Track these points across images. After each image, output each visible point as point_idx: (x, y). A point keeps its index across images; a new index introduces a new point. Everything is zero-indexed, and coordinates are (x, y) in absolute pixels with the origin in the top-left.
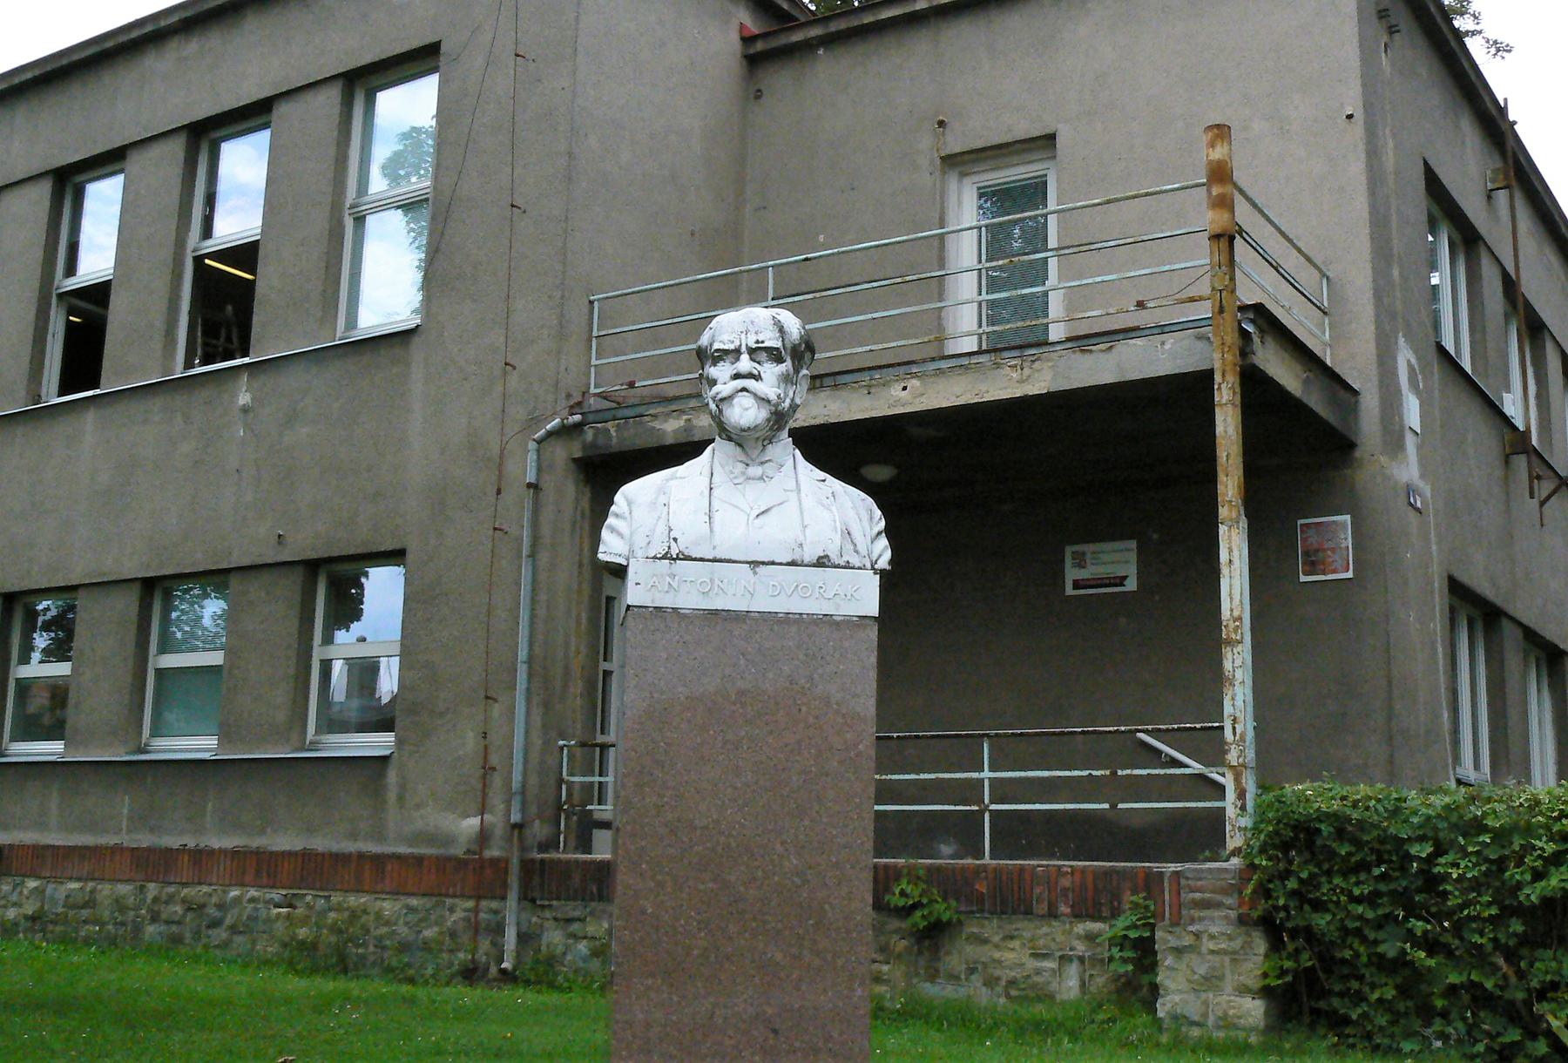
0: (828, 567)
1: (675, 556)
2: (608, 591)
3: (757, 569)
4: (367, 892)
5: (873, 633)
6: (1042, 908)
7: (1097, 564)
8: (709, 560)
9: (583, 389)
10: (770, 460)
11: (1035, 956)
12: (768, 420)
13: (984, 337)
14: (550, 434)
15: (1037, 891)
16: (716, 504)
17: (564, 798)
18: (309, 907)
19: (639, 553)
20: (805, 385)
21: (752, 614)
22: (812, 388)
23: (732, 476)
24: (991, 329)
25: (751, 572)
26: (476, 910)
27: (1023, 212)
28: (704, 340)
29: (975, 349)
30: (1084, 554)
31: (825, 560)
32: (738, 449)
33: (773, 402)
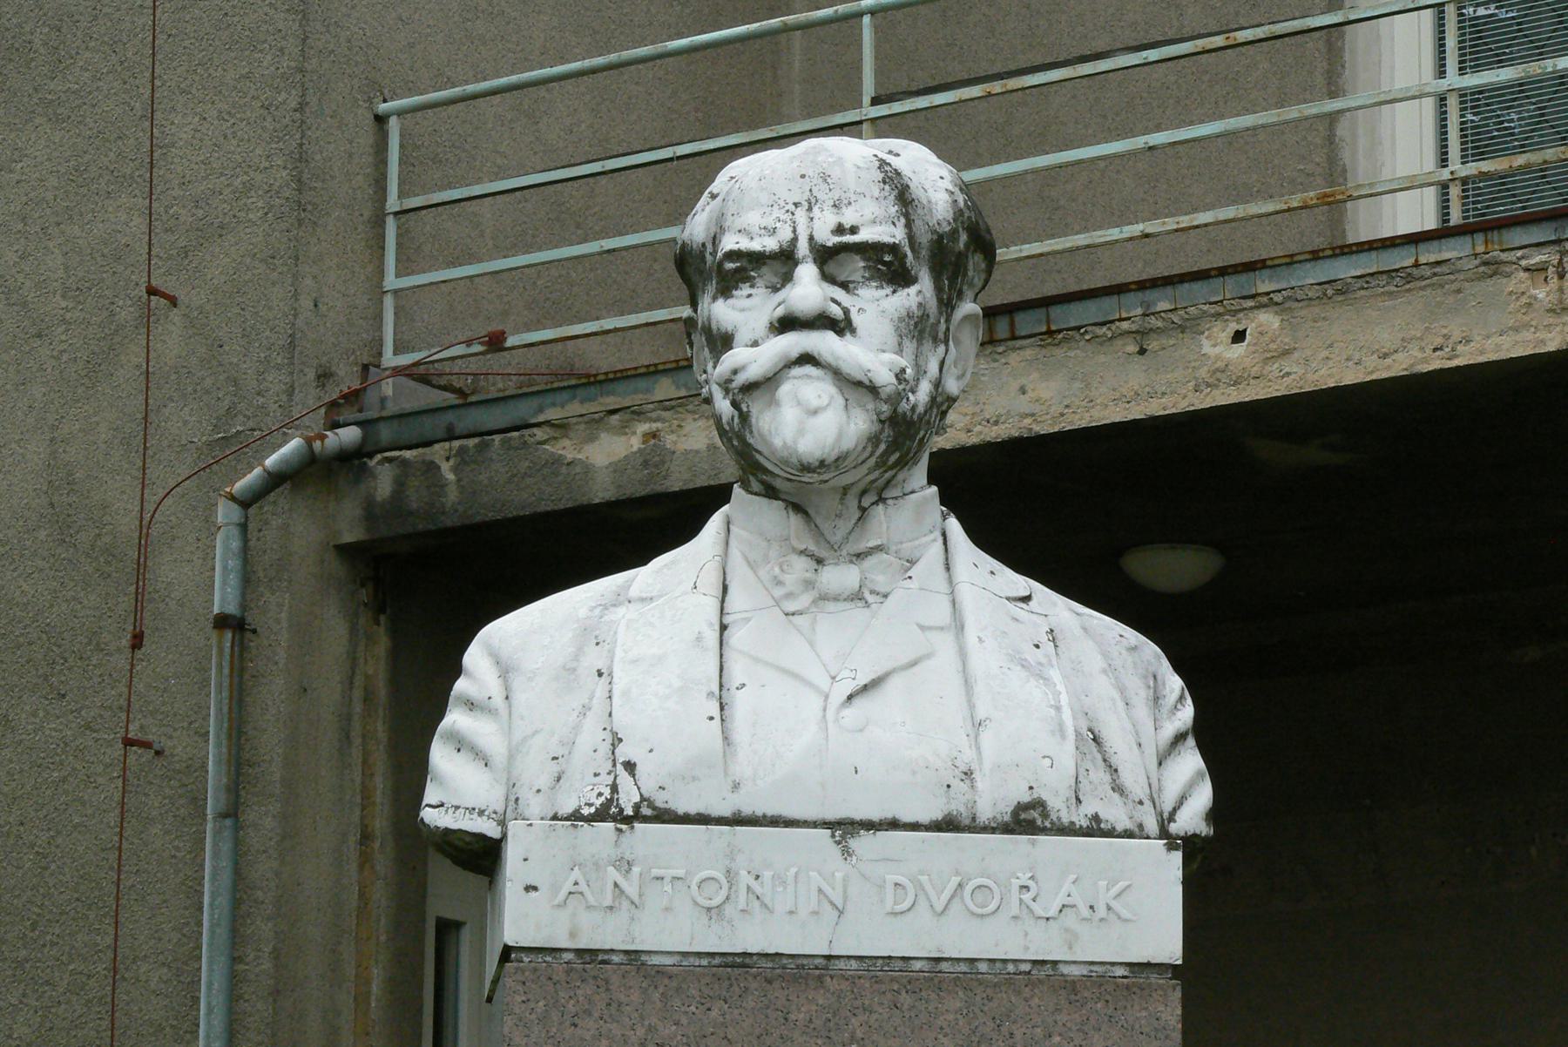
0: (1043, 831)
1: (629, 811)
2: (441, 905)
3: (853, 843)
5: (1170, 1010)
8: (721, 821)
10: (879, 548)
12: (874, 440)
13: (1455, 191)
14: (276, 480)
16: (737, 672)
19: (535, 806)
20: (969, 340)
21: (841, 964)
22: (989, 342)
24: (1472, 168)
25: (835, 851)
27: (1554, 208)
28: (697, 227)
29: (1431, 223)
31: (1034, 814)
32: (795, 520)
33: (884, 393)
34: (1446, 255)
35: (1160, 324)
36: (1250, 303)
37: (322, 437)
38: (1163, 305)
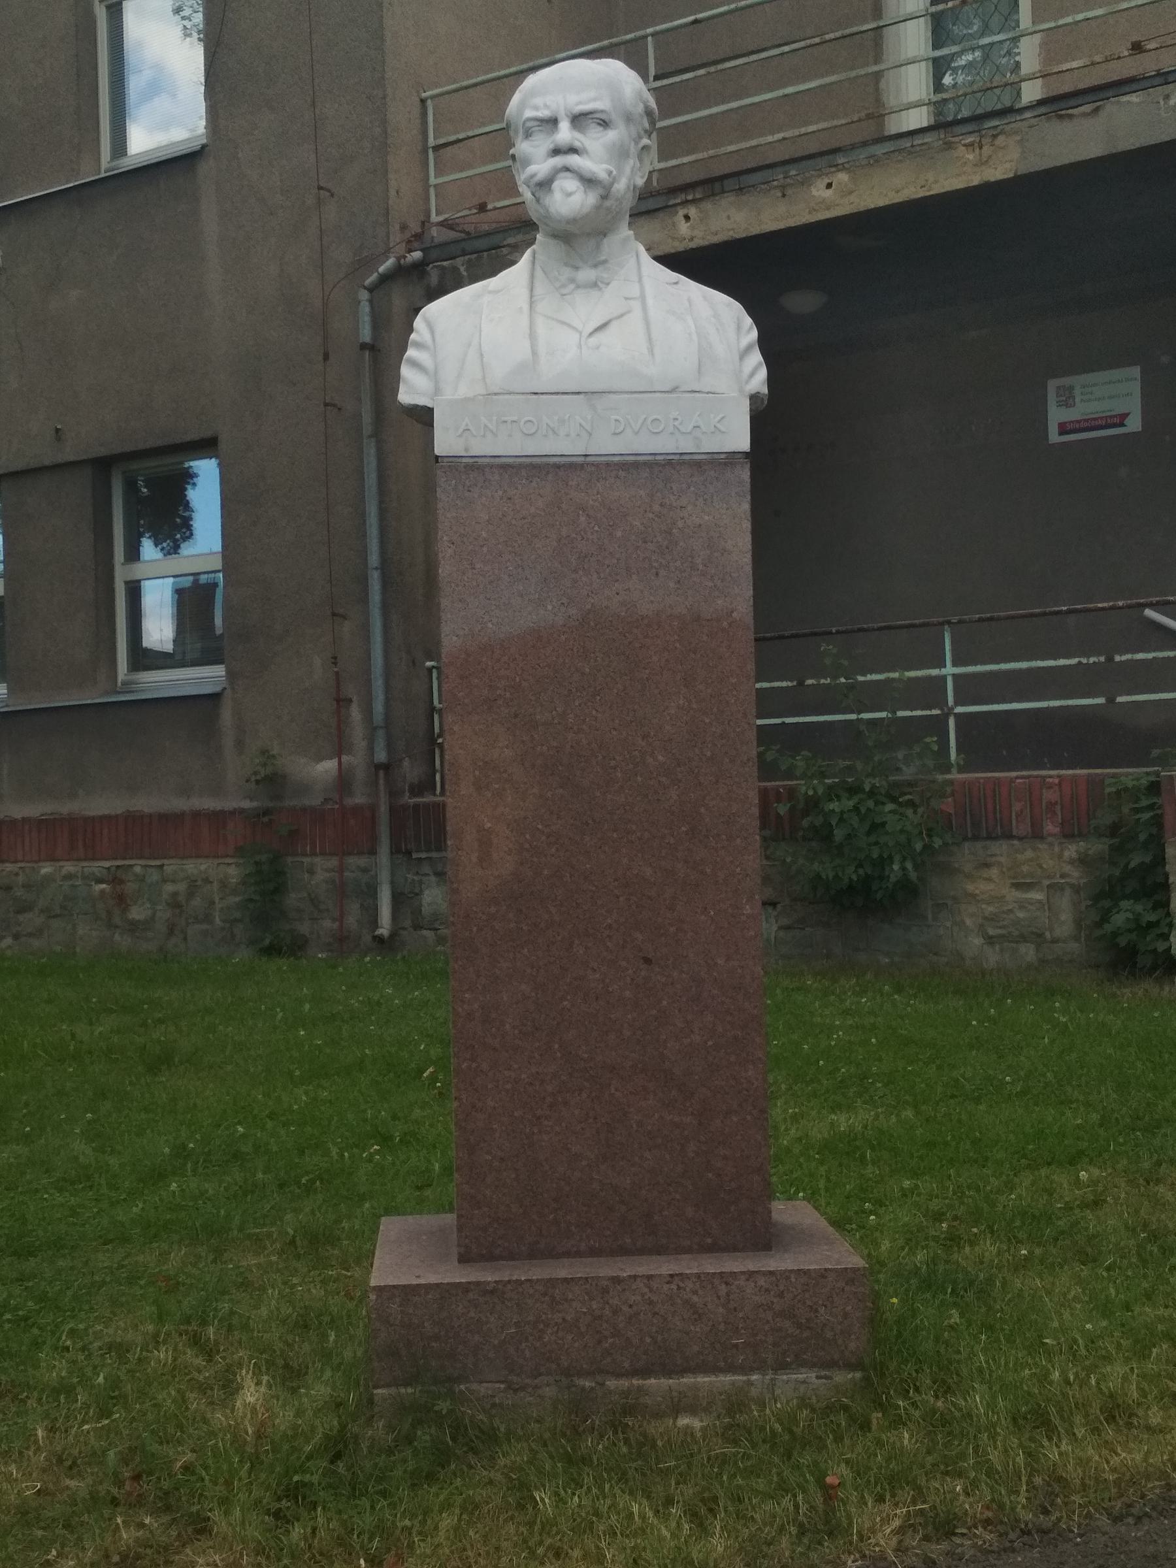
4: (207, 857)
5: (745, 474)
6: (1022, 828)
7: (1089, 400)
9: (422, 218)
11: (1017, 886)
14: (385, 279)
15: (1017, 807)
17: (437, 730)
18: (141, 879)
23: (558, 284)
26: (341, 869)
30: (1071, 388)
34: (926, 140)
35: (792, 182)
36: (833, 169)
37: (405, 257)
38: (793, 173)
